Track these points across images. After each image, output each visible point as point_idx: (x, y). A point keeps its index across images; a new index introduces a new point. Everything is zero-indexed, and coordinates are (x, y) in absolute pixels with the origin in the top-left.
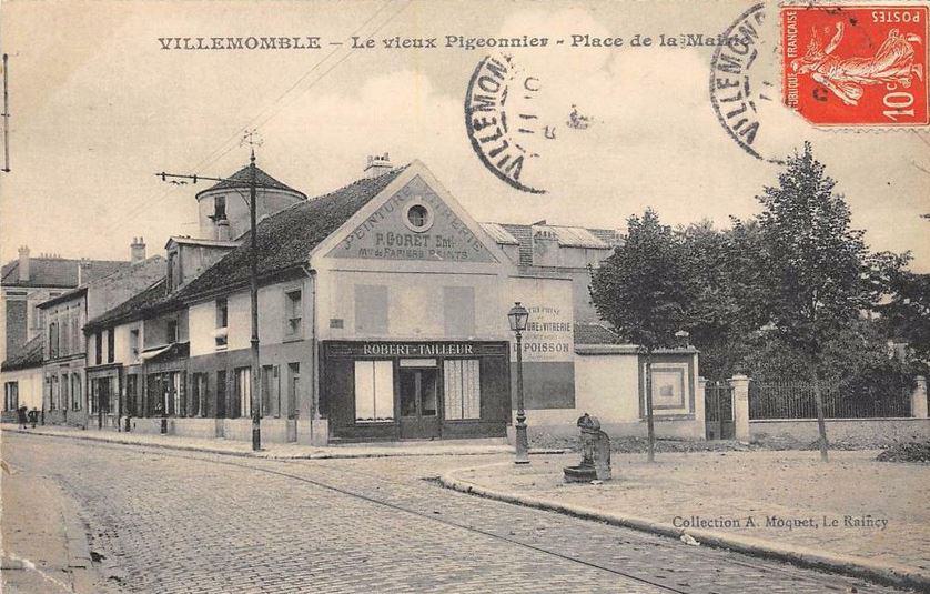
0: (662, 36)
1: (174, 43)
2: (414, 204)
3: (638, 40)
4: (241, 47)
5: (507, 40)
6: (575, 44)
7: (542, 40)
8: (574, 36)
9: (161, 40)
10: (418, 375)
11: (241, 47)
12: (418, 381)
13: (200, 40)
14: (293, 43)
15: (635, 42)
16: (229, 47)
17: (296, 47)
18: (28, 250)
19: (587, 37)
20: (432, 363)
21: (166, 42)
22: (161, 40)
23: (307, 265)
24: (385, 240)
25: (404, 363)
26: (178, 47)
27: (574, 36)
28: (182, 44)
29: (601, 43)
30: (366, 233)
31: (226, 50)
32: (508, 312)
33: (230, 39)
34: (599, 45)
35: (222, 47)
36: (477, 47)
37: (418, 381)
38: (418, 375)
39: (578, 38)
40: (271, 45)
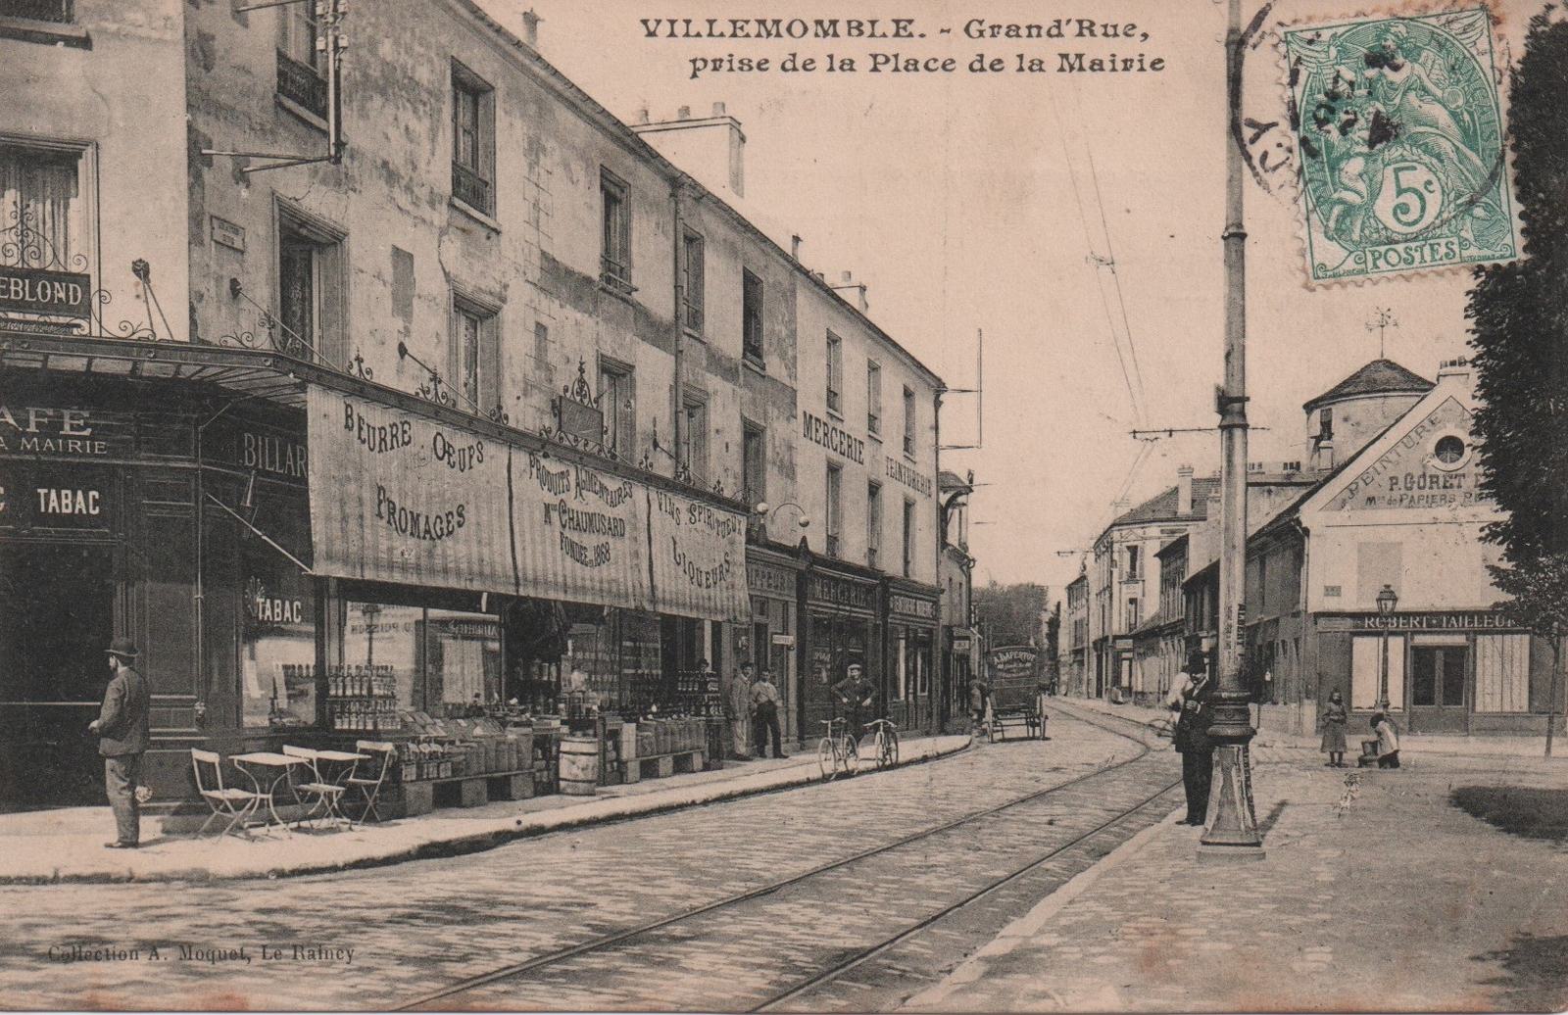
0: (831, 57)
1: (665, 28)
2: (1440, 435)
3: (981, 61)
4: (778, 35)
5: (1106, 34)
6: (875, 69)
7: (714, 61)
8: (875, 57)
9: (645, 22)
10: (1440, 654)
11: (778, 35)
12: (1439, 665)
13: (711, 22)
14: (867, 28)
15: (977, 66)
16: (759, 35)
17: (872, 35)
18: (1191, 470)
19: (896, 56)
20: (1460, 640)
21: (652, 25)
22: (645, 22)
23: (1299, 523)
24: (1401, 484)
25: (1420, 640)
26: (672, 34)
27: (875, 57)
28: (680, 28)
29: (920, 66)
30: (1377, 477)
31: (753, 40)
32: (1377, 596)
33: (762, 22)
34: (916, 69)
35: (748, 35)
36: (755, 69)
37: (1439, 665)
38: (1440, 654)
39: (881, 59)
40: (774, 32)
